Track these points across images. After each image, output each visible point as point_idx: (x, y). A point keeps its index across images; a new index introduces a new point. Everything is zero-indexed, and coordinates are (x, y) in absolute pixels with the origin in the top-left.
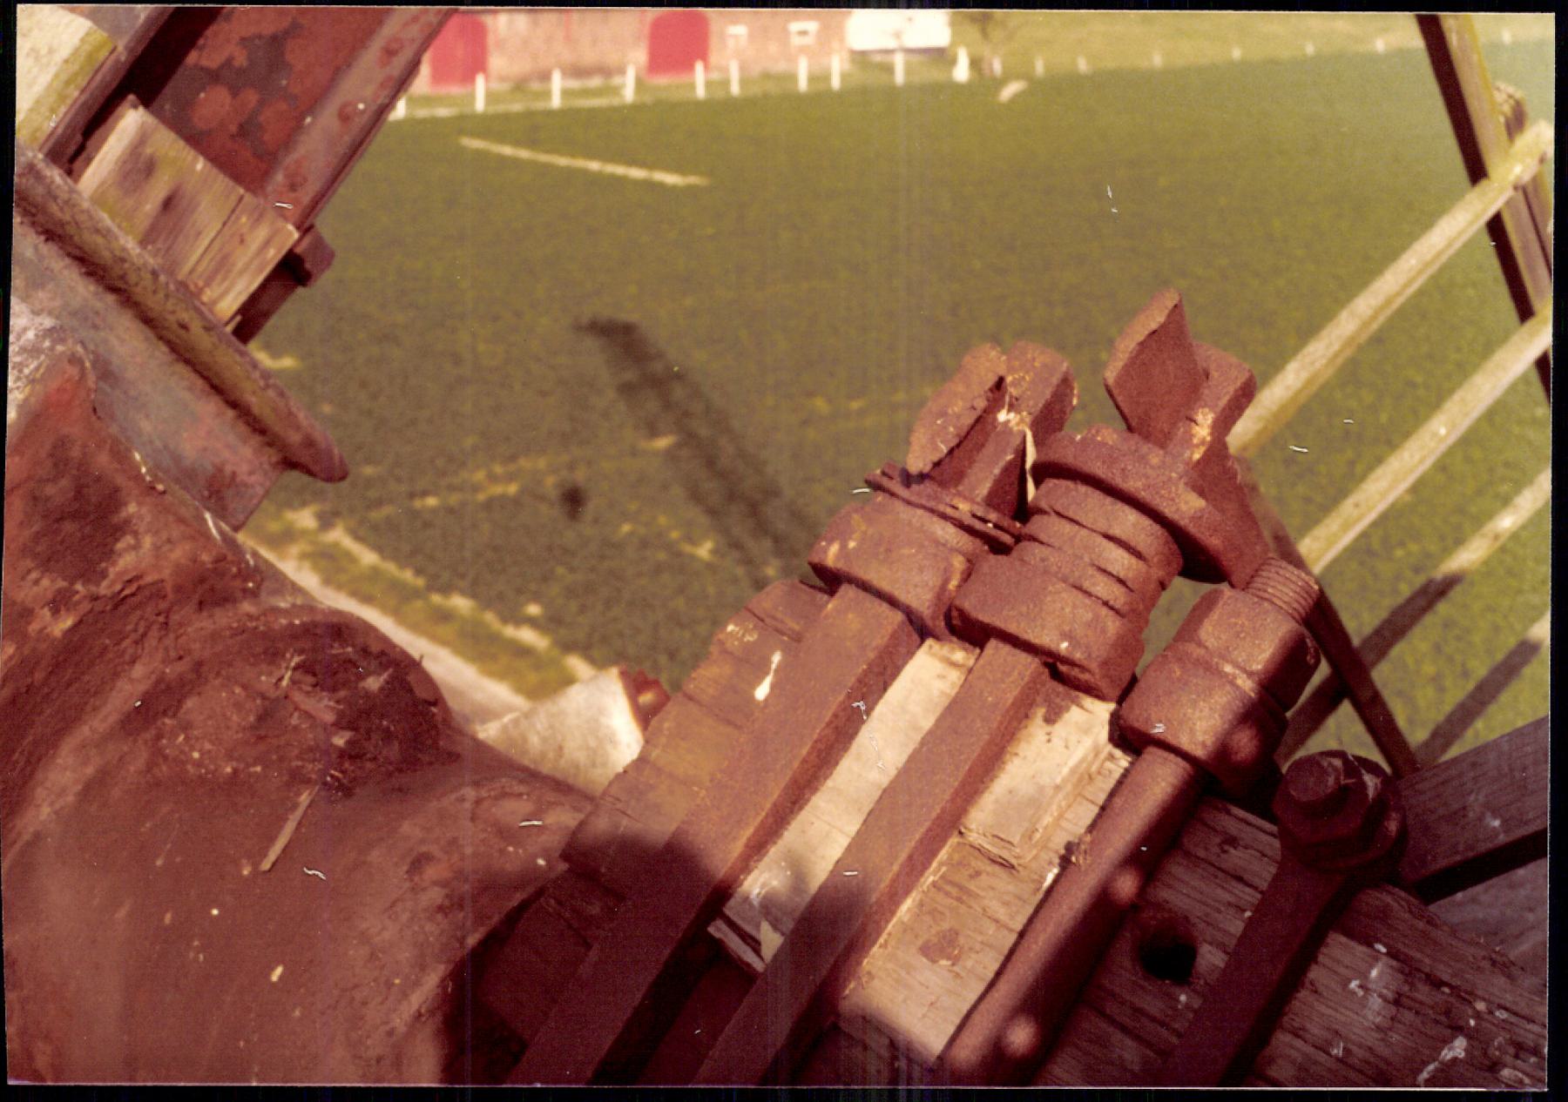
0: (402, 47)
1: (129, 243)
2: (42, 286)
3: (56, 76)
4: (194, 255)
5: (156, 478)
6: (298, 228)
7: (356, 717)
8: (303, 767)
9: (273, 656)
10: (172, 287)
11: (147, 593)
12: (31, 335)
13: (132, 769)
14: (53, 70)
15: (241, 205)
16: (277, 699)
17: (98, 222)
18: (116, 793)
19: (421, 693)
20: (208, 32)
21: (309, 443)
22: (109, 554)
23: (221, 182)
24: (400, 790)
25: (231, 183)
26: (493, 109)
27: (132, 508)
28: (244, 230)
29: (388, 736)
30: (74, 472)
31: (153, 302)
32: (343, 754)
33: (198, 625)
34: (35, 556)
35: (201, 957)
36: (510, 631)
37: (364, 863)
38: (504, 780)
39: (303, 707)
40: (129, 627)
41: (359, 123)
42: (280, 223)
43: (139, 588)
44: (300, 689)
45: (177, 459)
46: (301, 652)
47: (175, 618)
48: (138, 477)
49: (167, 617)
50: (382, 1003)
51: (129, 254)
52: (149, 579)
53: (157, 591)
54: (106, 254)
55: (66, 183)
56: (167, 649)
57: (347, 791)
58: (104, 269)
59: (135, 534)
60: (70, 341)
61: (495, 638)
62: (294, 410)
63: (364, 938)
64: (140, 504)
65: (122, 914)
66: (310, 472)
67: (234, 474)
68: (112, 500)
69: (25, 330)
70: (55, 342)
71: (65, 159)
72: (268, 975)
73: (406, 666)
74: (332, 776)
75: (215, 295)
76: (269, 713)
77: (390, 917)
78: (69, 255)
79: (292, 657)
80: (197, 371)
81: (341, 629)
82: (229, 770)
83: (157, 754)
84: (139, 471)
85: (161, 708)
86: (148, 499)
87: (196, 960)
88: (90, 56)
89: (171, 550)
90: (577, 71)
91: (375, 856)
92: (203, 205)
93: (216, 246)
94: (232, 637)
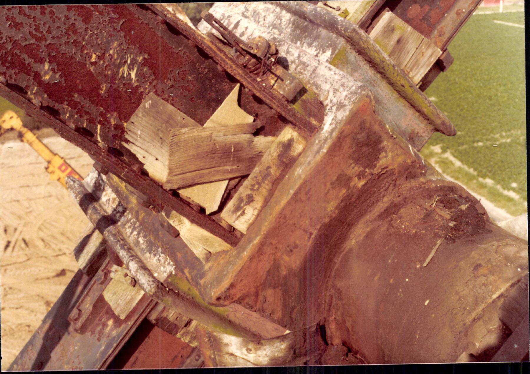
1: (385, 56)
4: (407, 60)
5: (393, 133)
6: (442, 50)
7: (458, 217)
8: (439, 232)
9: (430, 197)
10: (399, 72)
11: (389, 173)
12: (354, 88)
13: (382, 230)
16: (431, 211)
18: (377, 237)
19: (480, 211)
21: (444, 123)
22: (377, 159)
23: (416, 34)
24: (471, 241)
26: (505, 12)
27: (385, 143)
28: (424, 51)
29: (468, 224)
30: (367, 131)
31: (393, 77)
32: (452, 228)
33: (405, 185)
34: (353, 159)
35: (402, 295)
36: (506, 192)
37: (458, 266)
38: (507, 240)
39: (439, 213)
40: (383, 185)
41: (463, 16)
42: (436, 48)
43: (386, 171)
44: (439, 208)
45: (399, 128)
46: (439, 196)
47: (398, 182)
48: (388, 133)
49: (395, 182)
50: (462, 315)
52: (390, 168)
53: (392, 173)
54: (378, 59)
56: (395, 193)
57: (454, 241)
58: (377, 65)
59: (386, 152)
60: (367, 90)
61: (500, 195)
62: (439, 113)
63: (457, 293)
64: (388, 142)
65: (376, 278)
66: (443, 133)
67: (418, 133)
68: (379, 140)
69: (352, 86)
70: (362, 91)
72: (424, 303)
73: (475, 202)
74: (448, 235)
75: (413, 75)
76: (428, 215)
77: (466, 286)
79: (436, 197)
81: (452, 189)
82: (414, 231)
83: (390, 225)
84: (388, 131)
85: (393, 211)
86: (391, 140)
87: (400, 295)
89: (398, 158)
91: (462, 263)
92: (410, 42)
93: (414, 57)
94: (416, 190)
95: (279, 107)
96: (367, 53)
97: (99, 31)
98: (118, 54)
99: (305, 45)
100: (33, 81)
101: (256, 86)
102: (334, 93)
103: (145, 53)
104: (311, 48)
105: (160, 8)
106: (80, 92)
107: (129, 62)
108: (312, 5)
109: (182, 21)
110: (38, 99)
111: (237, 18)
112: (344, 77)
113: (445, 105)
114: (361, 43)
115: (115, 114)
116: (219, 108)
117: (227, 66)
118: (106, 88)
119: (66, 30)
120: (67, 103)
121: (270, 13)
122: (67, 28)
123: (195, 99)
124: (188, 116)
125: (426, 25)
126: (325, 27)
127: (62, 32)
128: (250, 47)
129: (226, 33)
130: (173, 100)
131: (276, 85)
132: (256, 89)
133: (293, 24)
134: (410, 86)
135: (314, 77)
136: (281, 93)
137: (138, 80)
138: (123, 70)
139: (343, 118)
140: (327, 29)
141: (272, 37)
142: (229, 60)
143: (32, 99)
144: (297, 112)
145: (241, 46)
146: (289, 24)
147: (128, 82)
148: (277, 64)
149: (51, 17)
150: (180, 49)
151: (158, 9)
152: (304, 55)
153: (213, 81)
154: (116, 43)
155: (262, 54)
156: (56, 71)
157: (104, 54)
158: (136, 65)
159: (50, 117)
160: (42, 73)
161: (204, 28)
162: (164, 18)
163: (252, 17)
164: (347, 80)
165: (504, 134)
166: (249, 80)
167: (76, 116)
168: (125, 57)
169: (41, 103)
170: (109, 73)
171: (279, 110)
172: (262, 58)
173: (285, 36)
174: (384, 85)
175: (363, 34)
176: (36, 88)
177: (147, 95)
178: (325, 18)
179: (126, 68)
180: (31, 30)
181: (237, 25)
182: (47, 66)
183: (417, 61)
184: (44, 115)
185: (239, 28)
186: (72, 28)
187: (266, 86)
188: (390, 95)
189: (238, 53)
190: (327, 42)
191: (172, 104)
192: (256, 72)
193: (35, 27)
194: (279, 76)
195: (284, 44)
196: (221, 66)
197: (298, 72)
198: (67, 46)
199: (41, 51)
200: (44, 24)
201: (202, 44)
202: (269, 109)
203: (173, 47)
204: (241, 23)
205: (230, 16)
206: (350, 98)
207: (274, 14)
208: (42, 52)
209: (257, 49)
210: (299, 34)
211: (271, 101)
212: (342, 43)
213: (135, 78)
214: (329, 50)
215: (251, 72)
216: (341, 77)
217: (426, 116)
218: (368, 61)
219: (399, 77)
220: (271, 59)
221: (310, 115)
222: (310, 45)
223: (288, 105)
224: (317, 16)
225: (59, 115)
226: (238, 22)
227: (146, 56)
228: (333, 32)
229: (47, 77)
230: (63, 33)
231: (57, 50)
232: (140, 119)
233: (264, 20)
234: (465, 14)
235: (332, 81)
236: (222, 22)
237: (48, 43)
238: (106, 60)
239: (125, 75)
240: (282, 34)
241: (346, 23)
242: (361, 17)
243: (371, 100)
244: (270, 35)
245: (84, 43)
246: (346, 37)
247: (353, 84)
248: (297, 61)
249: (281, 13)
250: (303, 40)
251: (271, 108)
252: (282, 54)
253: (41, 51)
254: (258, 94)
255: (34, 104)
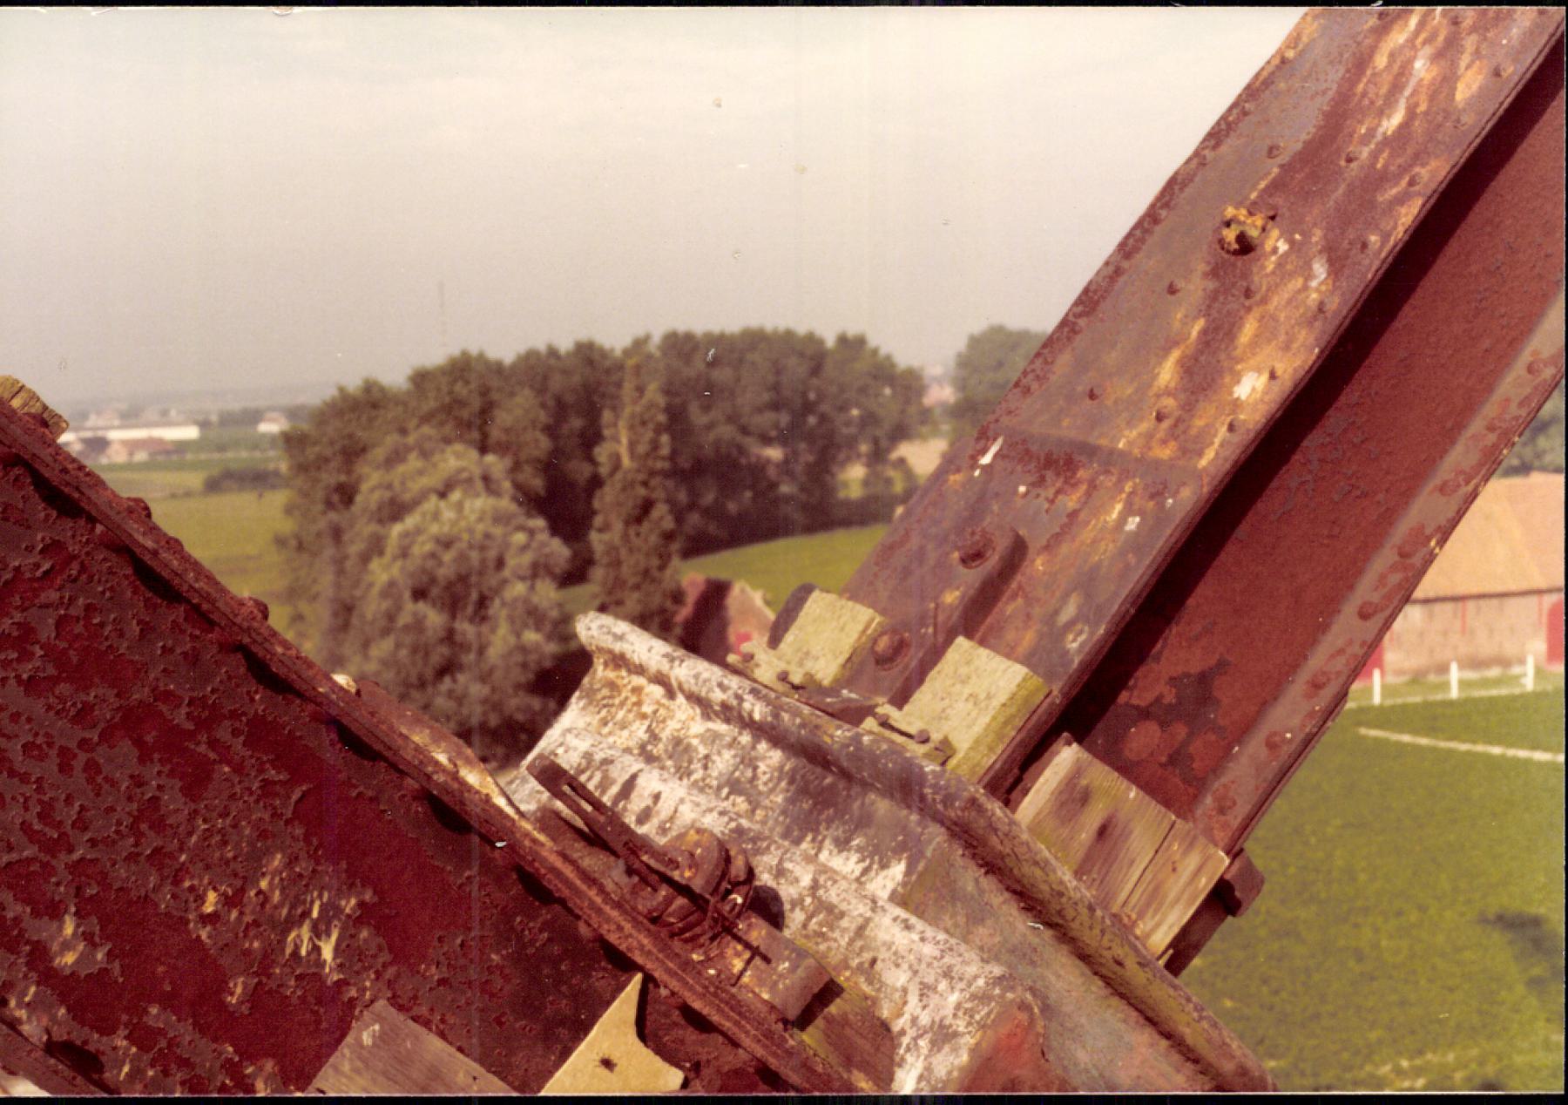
0: (1329, 680)
1: (1066, 875)
2: (982, 921)
3: (994, 718)
4: (1128, 884)
6: (1228, 853)
10: (1108, 922)
12: (981, 982)
14: (991, 713)
15: (1172, 832)
17: (1036, 854)
20: (1139, 673)
23: (1154, 808)
25: (1163, 809)
26: (1389, 702)
28: (1177, 857)
31: (1090, 938)
41: (1286, 751)
42: (1212, 849)
51: (1066, 888)
54: (1045, 887)
55: (1006, 816)
58: (1042, 902)
62: (1228, 1040)
69: (976, 977)
70: (1004, 990)
71: (1003, 790)
78: (1008, 889)
80: (1130, 1004)
88: (1026, 700)
90: (1474, 663)
92: (1136, 833)
93: (1149, 875)
95: (759, 1041)
96: (1011, 870)
97: (228, 821)
98: (283, 890)
99: (828, 843)
100: (24, 969)
101: (691, 982)
102: (922, 995)
103: (363, 886)
104: (845, 853)
105: (414, 757)
106: (168, 1002)
107: (315, 914)
108: (847, 726)
109: (477, 792)
110: (39, 1020)
111: (630, 766)
112: (951, 949)
113: (1225, 978)
114: (994, 841)
115: (269, 1065)
116: (583, 1046)
117: (606, 927)
118: (244, 988)
119: (131, 820)
120: (127, 1032)
121: (724, 747)
122: (136, 813)
123: (509, 1018)
124: (489, 1071)
125: (1177, 780)
126: (888, 793)
127: (119, 823)
128: (671, 861)
129: (602, 819)
130: (443, 1021)
131: (748, 973)
132: (691, 989)
133: (792, 782)
134: (1139, 963)
135: (862, 949)
136: (766, 996)
137: (341, 966)
138: (299, 936)
139: (949, 1073)
140: (892, 797)
141: (733, 825)
142: (612, 908)
143: (19, 1021)
144: (811, 1052)
145: (645, 858)
146: (780, 779)
147: (310, 971)
148: (750, 912)
149: (91, 780)
150: (467, 873)
151: (409, 758)
152: (829, 883)
153: (563, 968)
154: (279, 856)
155: (708, 882)
156: (97, 939)
157: (241, 891)
158: (336, 922)
159: (74, 1078)
160: (55, 947)
161: (530, 795)
162: (424, 784)
163: (670, 757)
164: (960, 959)
165: (1405, 1063)
166: (671, 965)
167: (151, 1073)
168: (305, 900)
169: (48, 1032)
170: (256, 944)
171: (760, 1052)
172: (708, 896)
173: (766, 816)
174: (1064, 960)
175: (999, 812)
176: (33, 989)
177: (367, 1006)
178: (886, 764)
179: (305, 932)
180: (28, 816)
181: (629, 786)
182: (69, 928)
183: (1157, 889)
184: (56, 1072)
185: (634, 796)
186: (151, 814)
187: (718, 975)
188: (1083, 989)
189: (636, 879)
190: (894, 838)
191: (442, 1035)
192: (687, 935)
193: (38, 809)
194: (758, 947)
195: (768, 848)
196: (589, 925)
197: (811, 933)
198: (133, 867)
199: (54, 880)
200: (69, 800)
201: (534, 860)
202: (730, 1048)
203: (449, 868)
204: (640, 781)
205: (607, 762)
206: (970, 1013)
207: (733, 752)
208: (58, 884)
209: (690, 867)
210: (811, 811)
211: (737, 1023)
212: (938, 839)
213: (334, 959)
214: (900, 860)
215: (672, 935)
216: (943, 951)
217: (1189, 1049)
218: (1014, 892)
219: (1106, 938)
220: (733, 896)
221: (849, 1062)
222: (842, 845)
223: (787, 1036)
224: (861, 759)
225: (100, 1068)
226: (634, 777)
227: (368, 896)
228: (909, 807)
229: (69, 958)
230: (122, 828)
231: (103, 880)
232: (344, 1080)
233: (706, 767)
234: (1293, 747)
235: (915, 963)
236: (583, 778)
237: (76, 856)
238: (247, 910)
239: (303, 952)
240: (758, 812)
241: (949, 780)
242: (988, 759)
243: (1032, 1020)
244: (726, 819)
245: (183, 858)
246: (948, 823)
247: (977, 971)
248: (808, 900)
249: (754, 748)
250: (821, 828)
251: (735, 1044)
252: (765, 878)
253: (54, 880)
254: (697, 1005)
255: (26, 1039)
